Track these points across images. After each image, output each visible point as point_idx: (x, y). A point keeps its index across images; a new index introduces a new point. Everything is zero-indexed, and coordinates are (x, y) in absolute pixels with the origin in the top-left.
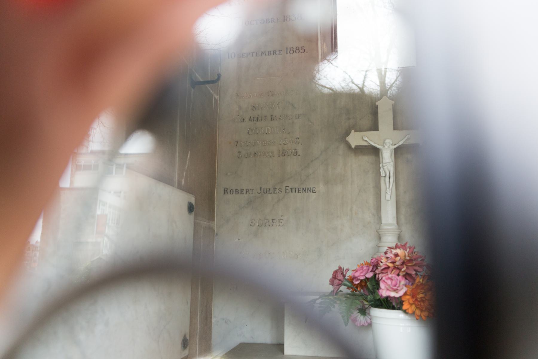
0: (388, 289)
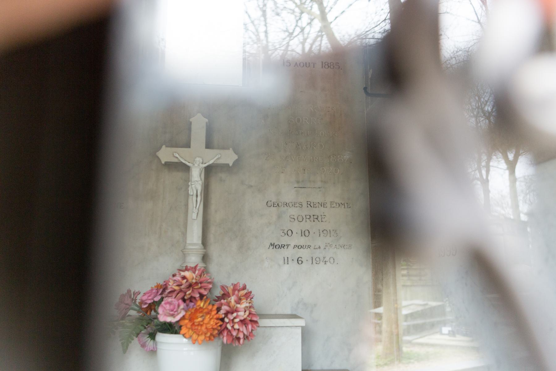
0: (165, 315)
